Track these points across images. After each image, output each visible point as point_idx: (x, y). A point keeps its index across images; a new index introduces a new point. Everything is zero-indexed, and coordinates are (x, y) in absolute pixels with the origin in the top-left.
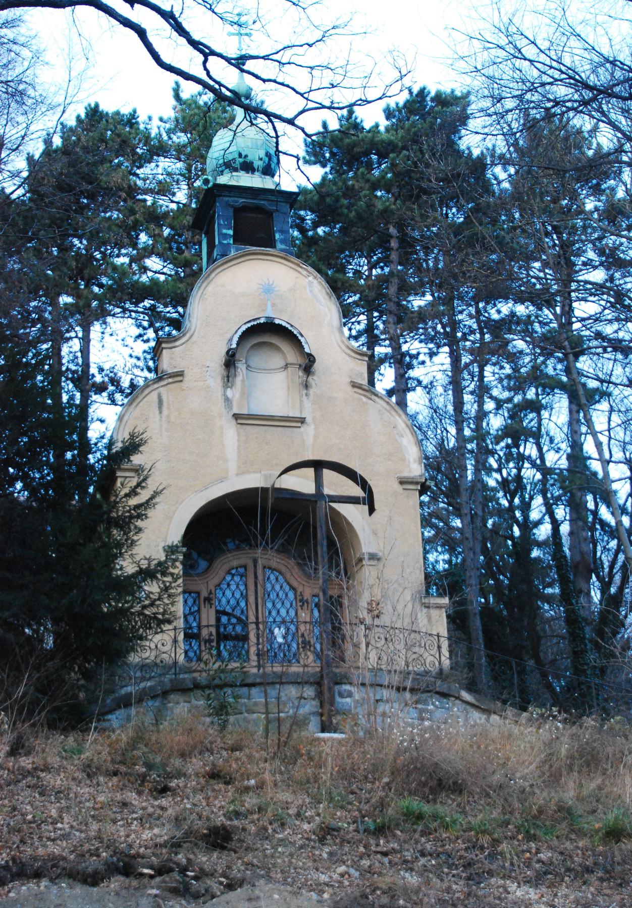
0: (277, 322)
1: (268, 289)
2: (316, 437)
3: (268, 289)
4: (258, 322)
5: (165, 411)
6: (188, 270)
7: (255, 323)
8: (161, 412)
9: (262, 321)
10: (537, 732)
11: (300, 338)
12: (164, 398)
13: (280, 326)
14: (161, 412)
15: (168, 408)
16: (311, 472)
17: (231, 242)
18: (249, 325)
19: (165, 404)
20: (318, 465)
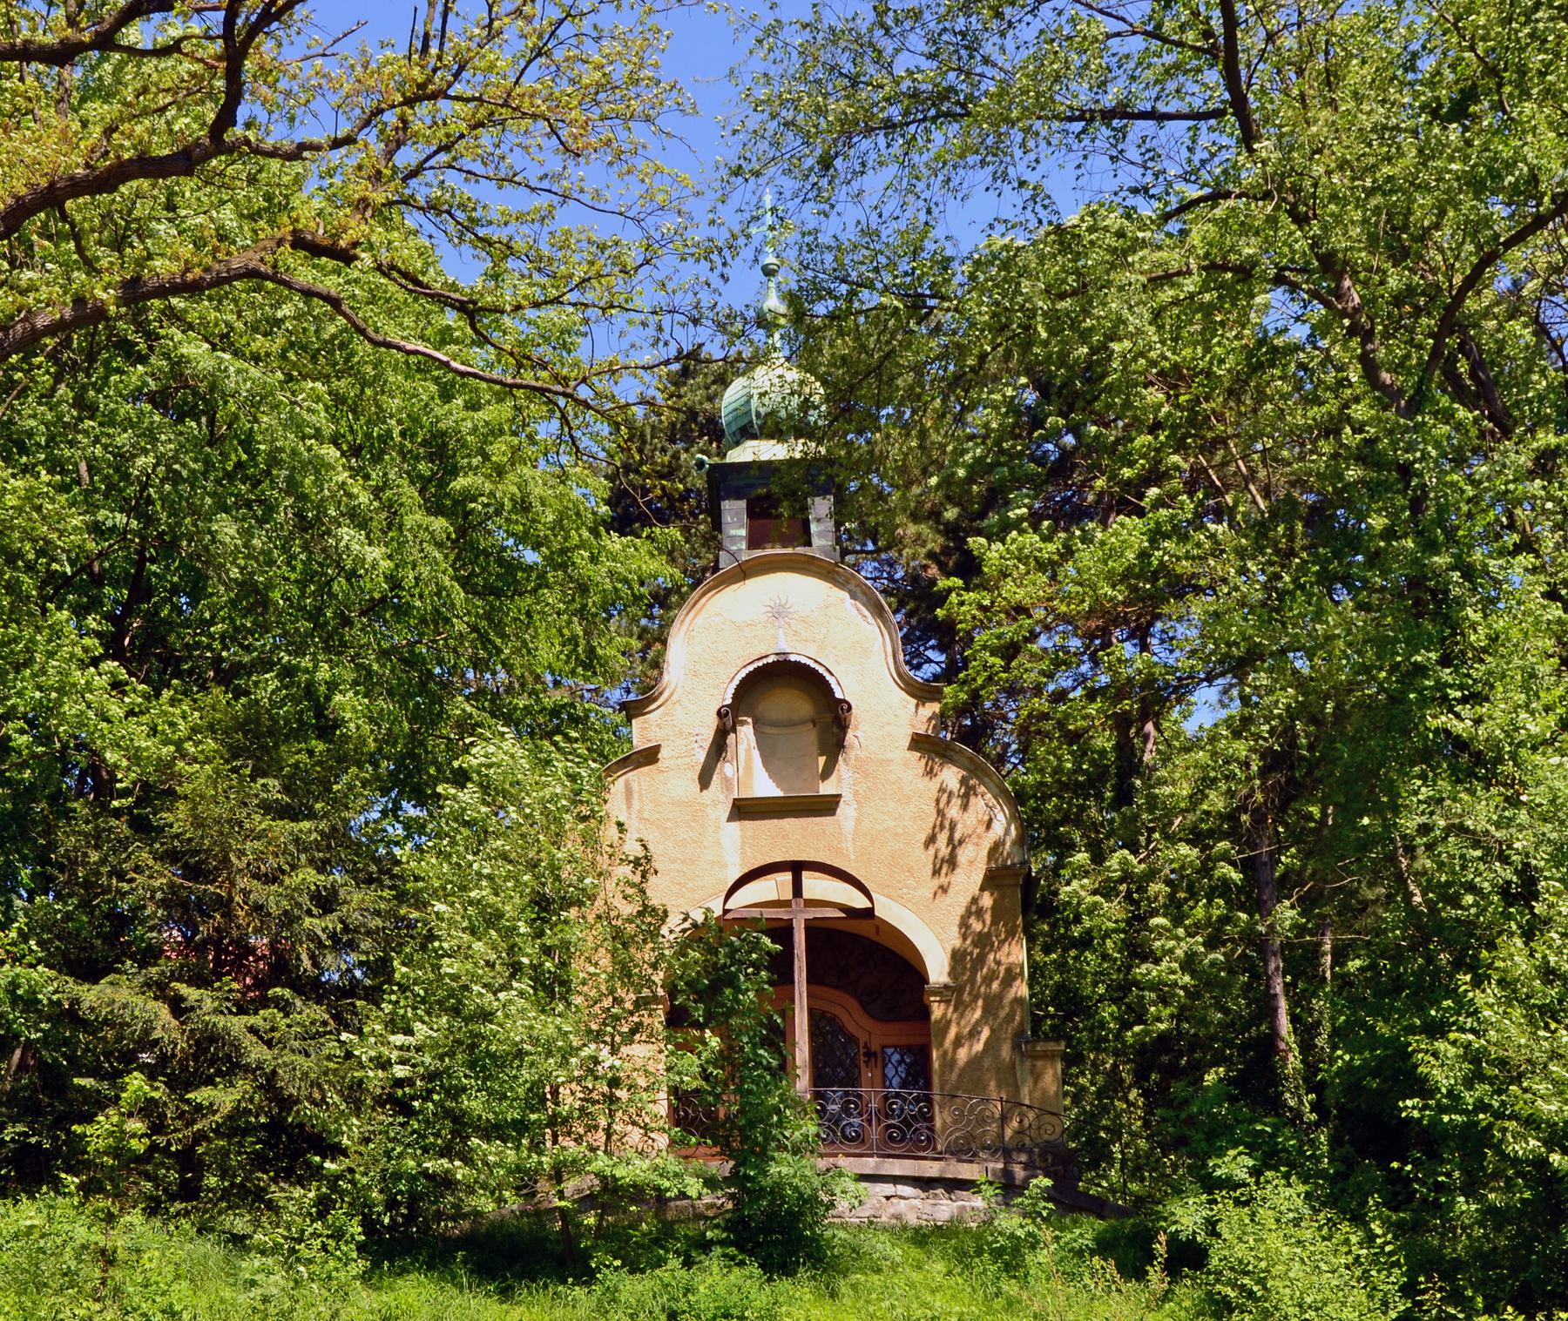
0: (793, 658)
1: (778, 613)
2: (859, 821)
3: (778, 613)
4: (765, 661)
5: (636, 805)
6: (1303, 511)
7: (760, 664)
8: (629, 807)
9: (770, 660)
10: (354, 1278)
11: (828, 677)
12: (635, 786)
13: (797, 663)
14: (629, 807)
15: (641, 800)
16: (787, 877)
17: (744, 546)
18: (751, 668)
19: (636, 796)
20: (796, 868)
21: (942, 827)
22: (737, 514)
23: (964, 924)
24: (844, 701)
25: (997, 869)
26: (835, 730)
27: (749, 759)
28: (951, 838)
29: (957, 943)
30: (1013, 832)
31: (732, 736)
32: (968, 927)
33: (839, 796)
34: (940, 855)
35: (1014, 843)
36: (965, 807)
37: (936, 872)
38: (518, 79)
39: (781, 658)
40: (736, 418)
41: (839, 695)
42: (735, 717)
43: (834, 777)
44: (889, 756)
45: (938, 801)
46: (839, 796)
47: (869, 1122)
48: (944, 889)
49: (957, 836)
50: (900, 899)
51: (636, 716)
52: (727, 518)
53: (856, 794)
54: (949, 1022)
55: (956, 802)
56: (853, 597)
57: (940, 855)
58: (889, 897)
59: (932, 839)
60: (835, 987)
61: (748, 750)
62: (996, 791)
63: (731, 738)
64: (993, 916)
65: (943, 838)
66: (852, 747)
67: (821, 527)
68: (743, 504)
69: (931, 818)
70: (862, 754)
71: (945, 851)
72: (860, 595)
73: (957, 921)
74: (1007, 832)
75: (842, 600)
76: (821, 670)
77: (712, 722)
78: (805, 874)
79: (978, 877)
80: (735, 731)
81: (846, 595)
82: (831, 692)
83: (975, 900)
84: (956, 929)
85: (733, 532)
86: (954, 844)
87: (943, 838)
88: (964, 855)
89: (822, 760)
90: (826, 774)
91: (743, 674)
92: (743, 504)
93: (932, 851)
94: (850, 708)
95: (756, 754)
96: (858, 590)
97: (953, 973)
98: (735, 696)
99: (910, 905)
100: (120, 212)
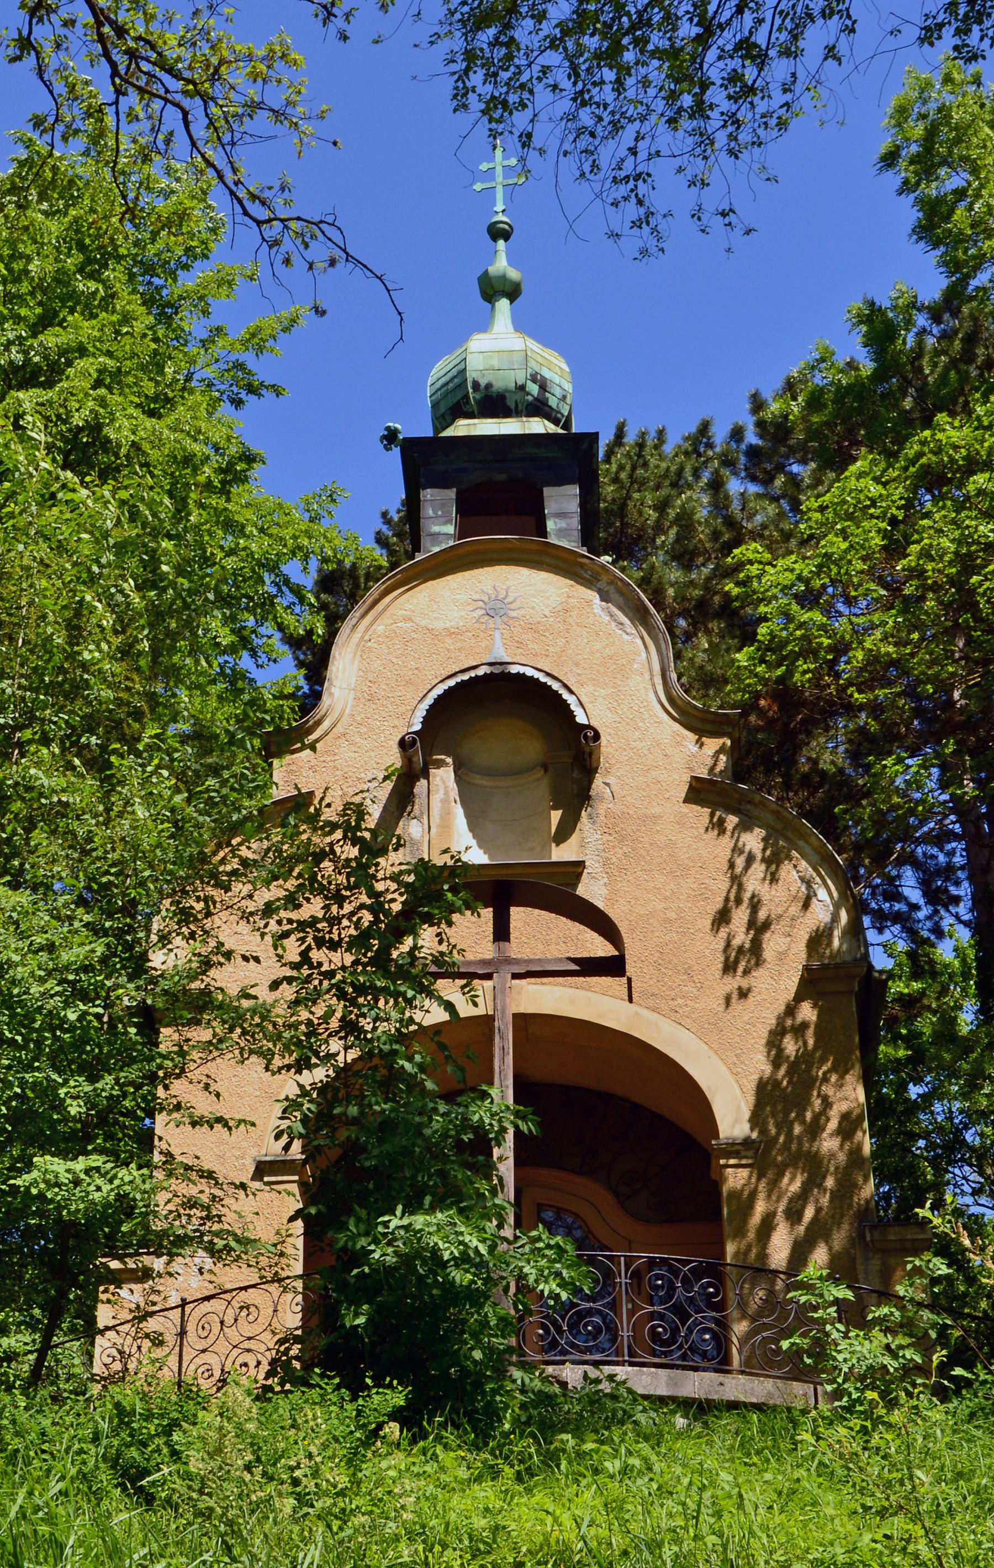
0: (514, 669)
9: (481, 672)
11: (566, 695)
18: (452, 683)
21: (739, 901)
22: (442, 506)
23: (774, 1041)
24: (589, 727)
25: (823, 967)
26: (576, 774)
27: (447, 815)
28: (752, 923)
29: (767, 1069)
30: (844, 916)
31: (423, 782)
32: (780, 1050)
33: (581, 864)
34: (736, 942)
35: (844, 934)
36: (774, 879)
37: (729, 968)
38: (233, 167)
39: (497, 670)
40: (445, 396)
41: (581, 718)
42: (427, 754)
43: (574, 839)
44: (656, 810)
45: (732, 865)
46: (581, 864)
47: (53, 705)
48: (743, 994)
49: (762, 915)
50: (673, 1015)
51: (279, 755)
52: (428, 511)
53: (606, 863)
54: (753, 1195)
55: (758, 869)
56: (605, 598)
57: (736, 942)
58: (654, 1010)
59: (722, 918)
60: (580, 1173)
61: (445, 801)
62: (816, 858)
63: (421, 785)
64: (817, 1034)
65: (740, 916)
66: (602, 799)
67: (562, 524)
68: (452, 493)
69: (722, 884)
70: (616, 808)
71: (742, 938)
72: (614, 595)
73: (762, 1034)
74: (835, 918)
75: (589, 603)
76: (555, 686)
77: (394, 758)
78: (518, 915)
79: (791, 983)
80: (427, 776)
81: (593, 596)
82: (571, 715)
83: (790, 1010)
84: (763, 1050)
85: (435, 529)
86: (759, 928)
87: (740, 916)
88: (772, 944)
89: (556, 816)
90: (563, 835)
91: (439, 690)
92: (452, 493)
93: (723, 933)
94: (597, 737)
95: (459, 811)
96: (612, 589)
97: (756, 1119)
98: (426, 721)
99: (687, 1022)
100: (143, 766)
